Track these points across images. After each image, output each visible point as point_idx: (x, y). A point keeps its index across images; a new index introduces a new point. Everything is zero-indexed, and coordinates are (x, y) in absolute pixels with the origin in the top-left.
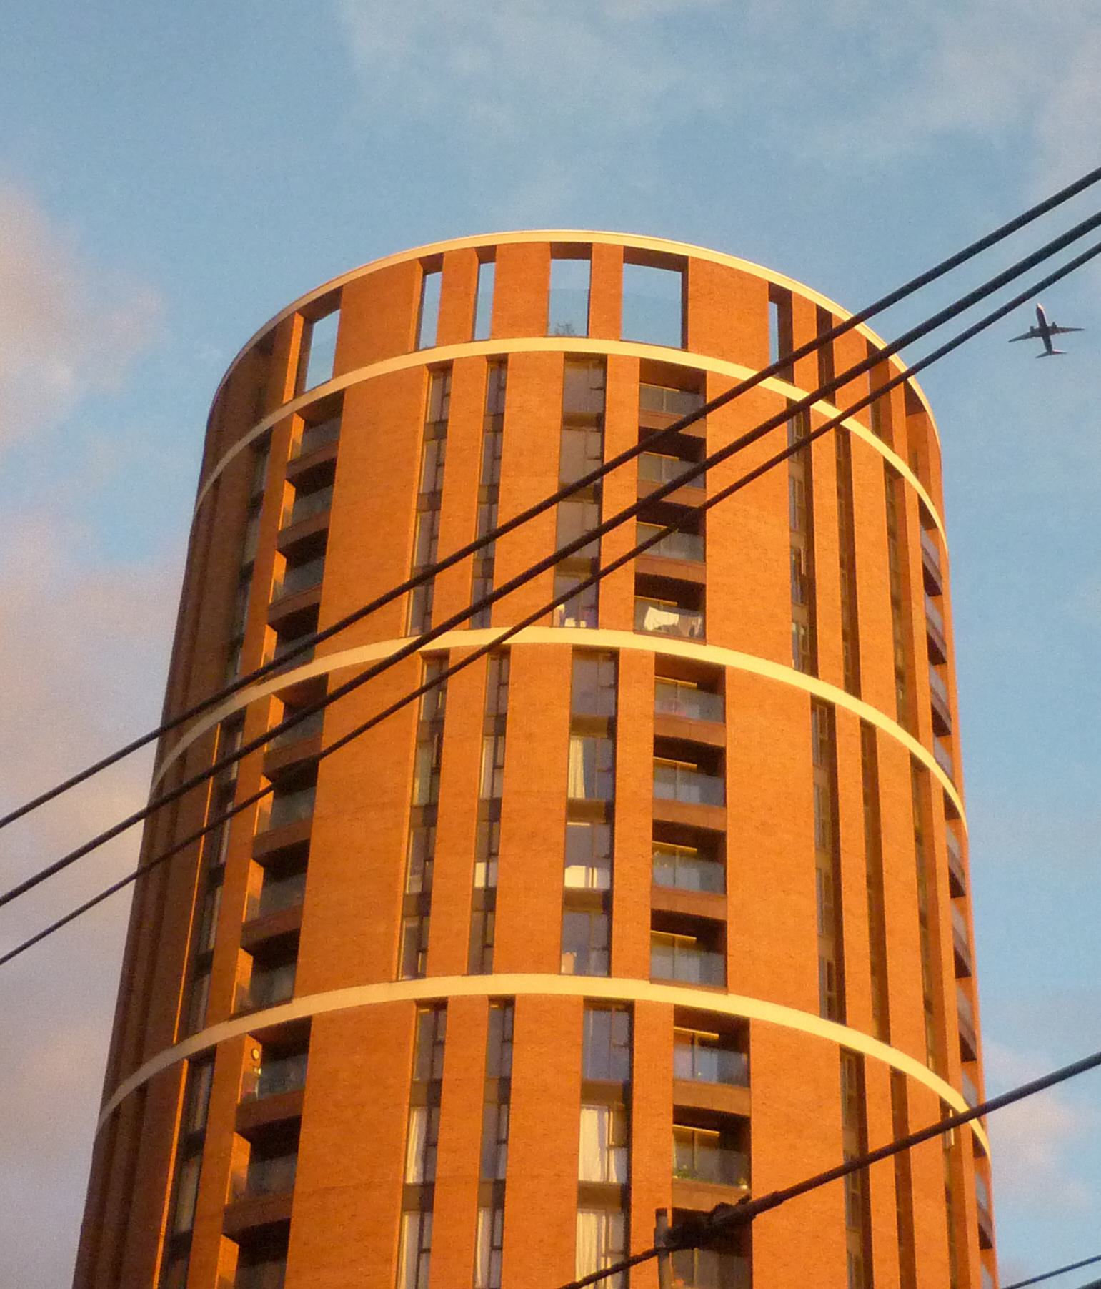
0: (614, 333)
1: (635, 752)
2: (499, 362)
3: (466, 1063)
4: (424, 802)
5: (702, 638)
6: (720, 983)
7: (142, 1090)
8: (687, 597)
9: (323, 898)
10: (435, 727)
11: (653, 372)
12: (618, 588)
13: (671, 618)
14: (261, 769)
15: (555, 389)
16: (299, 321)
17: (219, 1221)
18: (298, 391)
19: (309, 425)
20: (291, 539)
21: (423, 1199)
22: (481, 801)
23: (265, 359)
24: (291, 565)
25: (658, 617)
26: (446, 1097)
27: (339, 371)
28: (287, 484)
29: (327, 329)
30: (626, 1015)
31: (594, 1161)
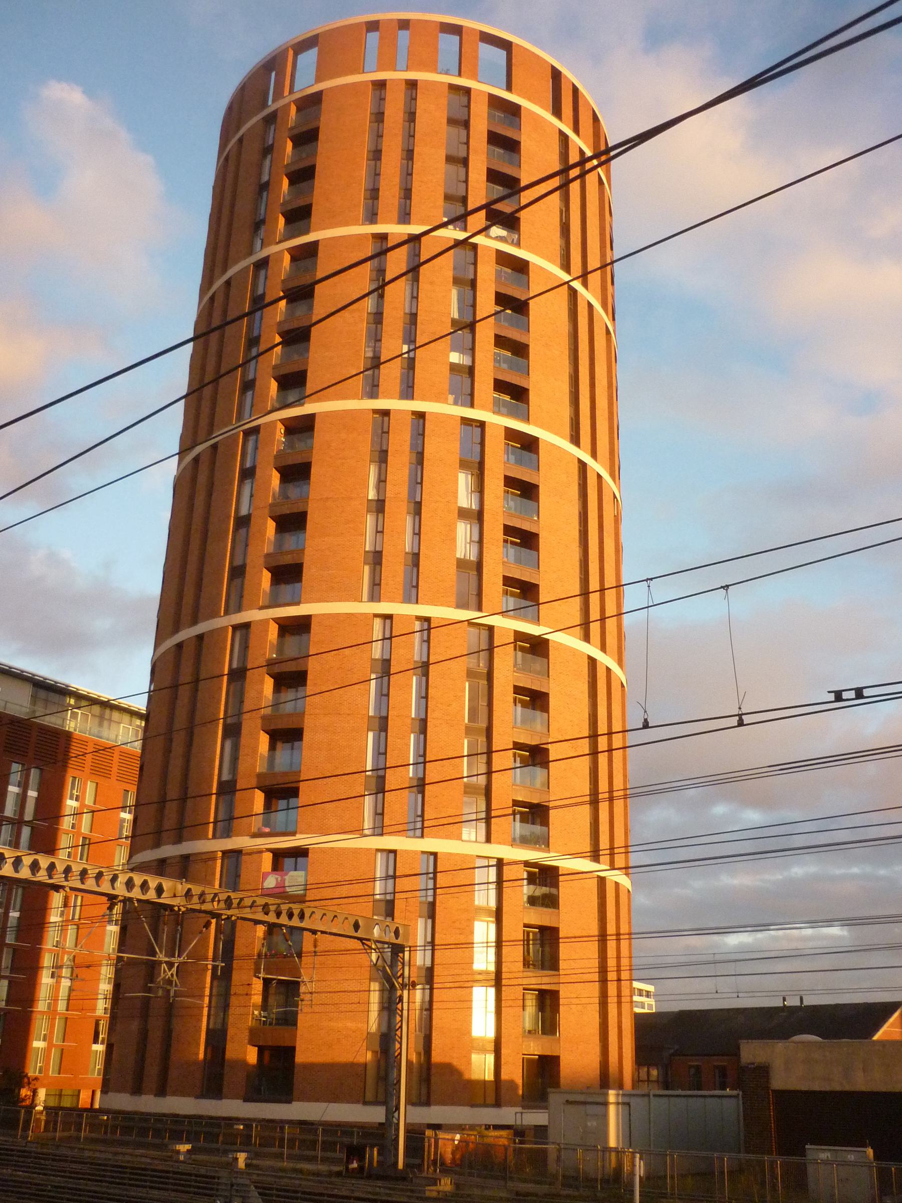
0: (474, 76)
1: (486, 304)
2: (412, 85)
3: (400, 442)
4: (374, 311)
5: (518, 244)
6: (527, 419)
7: (228, 283)
8: (511, 222)
9: (314, 546)
10: (378, 317)
11: (495, 102)
12: (478, 220)
13: (503, 233)
14: (259, 726)
15: (444, 102)
16: (291, 53)
17: (267, 511)
18: (291, 91)
19: (299, 110)
20: (296, 132)
21: (379, 506)
22: (405, 314)
23: (273, 65)
24: (291, 183)
25: (496, 231)
26: (390, 458)
27: (319, 79)
28: (267, 676)
29: (309, 59)
30: (479, 429)
31: (465, 499)
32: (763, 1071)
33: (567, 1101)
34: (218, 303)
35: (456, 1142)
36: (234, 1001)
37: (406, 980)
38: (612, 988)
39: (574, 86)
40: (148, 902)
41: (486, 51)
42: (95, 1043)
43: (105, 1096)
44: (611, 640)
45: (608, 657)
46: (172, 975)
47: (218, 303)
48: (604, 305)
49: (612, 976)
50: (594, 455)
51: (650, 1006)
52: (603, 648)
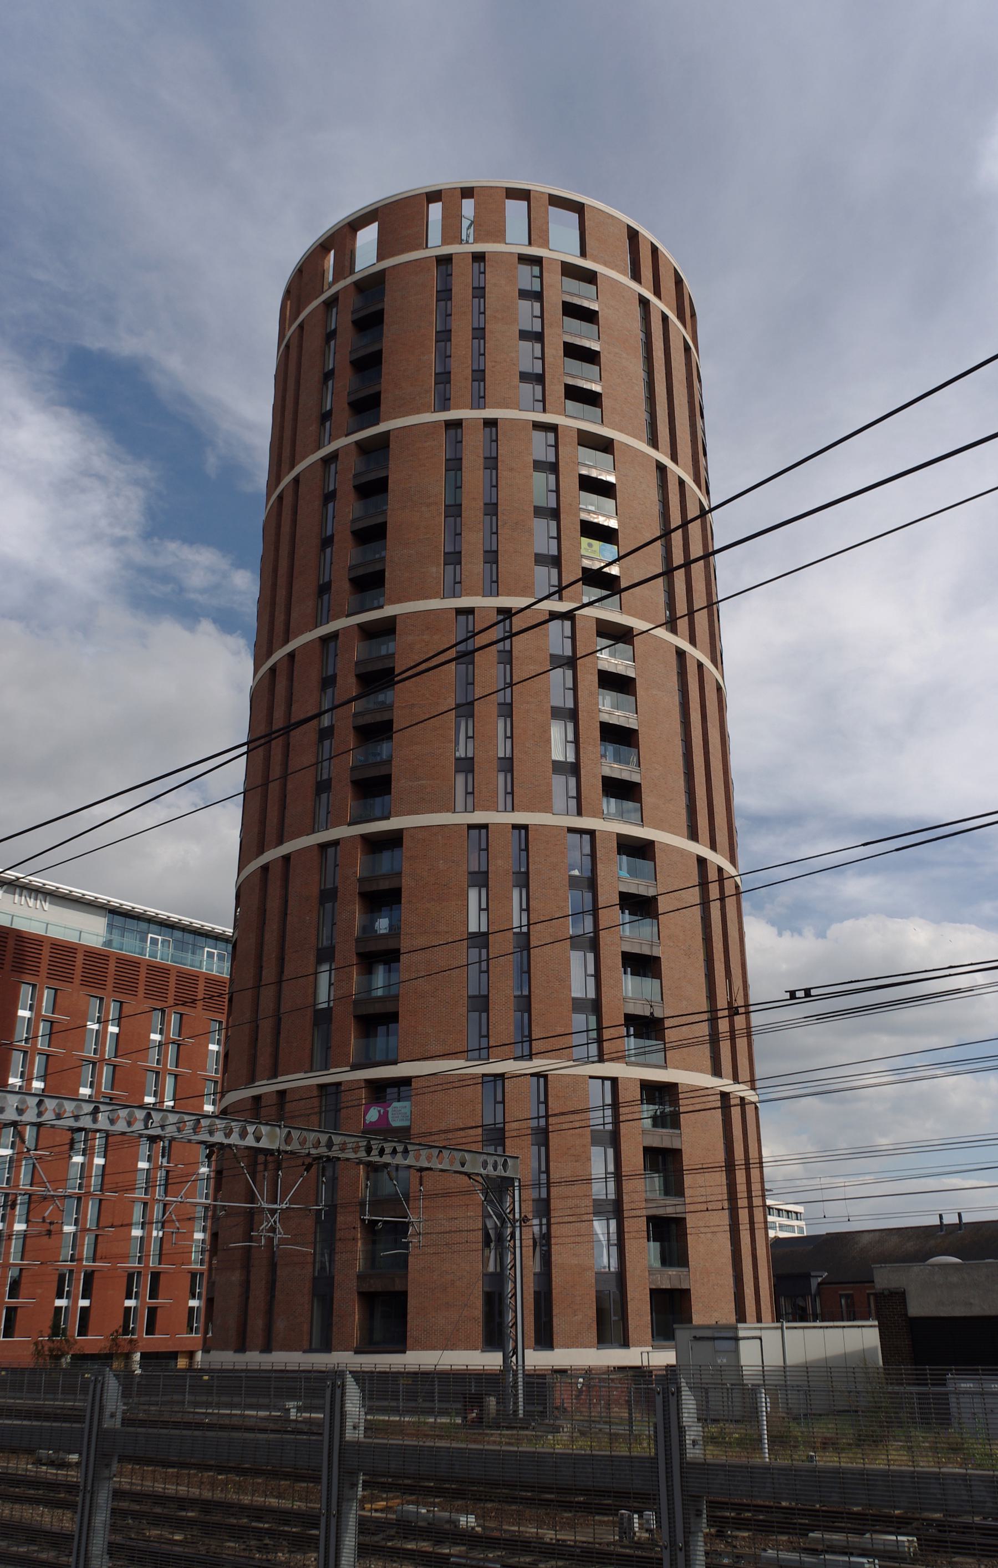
32: (899, 1297)
33: (695, 1337)
34: (288, 501)
35: (579, 1386)
36: (339, 1246)
37: (517, 1216)
38: (743, 1215)
39: (653, 246)
40: (248, 1148)
41: (555, 213)
42: (127, 1298)
43: (206, 1355)
44: (722, 837)
45: (719, 856)
46: (275, 1222)
47: (288, 501)
48: (697, 481)
49: (743, 1203)
50: (693, 641)
51: (801, 1229)
52: (713, 847)
